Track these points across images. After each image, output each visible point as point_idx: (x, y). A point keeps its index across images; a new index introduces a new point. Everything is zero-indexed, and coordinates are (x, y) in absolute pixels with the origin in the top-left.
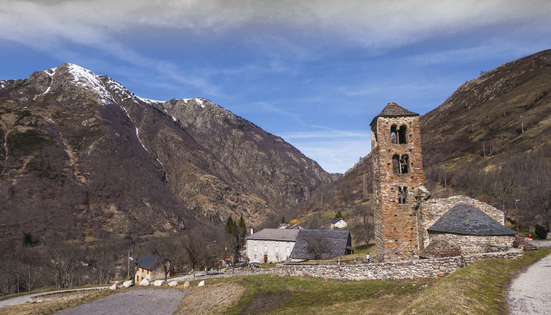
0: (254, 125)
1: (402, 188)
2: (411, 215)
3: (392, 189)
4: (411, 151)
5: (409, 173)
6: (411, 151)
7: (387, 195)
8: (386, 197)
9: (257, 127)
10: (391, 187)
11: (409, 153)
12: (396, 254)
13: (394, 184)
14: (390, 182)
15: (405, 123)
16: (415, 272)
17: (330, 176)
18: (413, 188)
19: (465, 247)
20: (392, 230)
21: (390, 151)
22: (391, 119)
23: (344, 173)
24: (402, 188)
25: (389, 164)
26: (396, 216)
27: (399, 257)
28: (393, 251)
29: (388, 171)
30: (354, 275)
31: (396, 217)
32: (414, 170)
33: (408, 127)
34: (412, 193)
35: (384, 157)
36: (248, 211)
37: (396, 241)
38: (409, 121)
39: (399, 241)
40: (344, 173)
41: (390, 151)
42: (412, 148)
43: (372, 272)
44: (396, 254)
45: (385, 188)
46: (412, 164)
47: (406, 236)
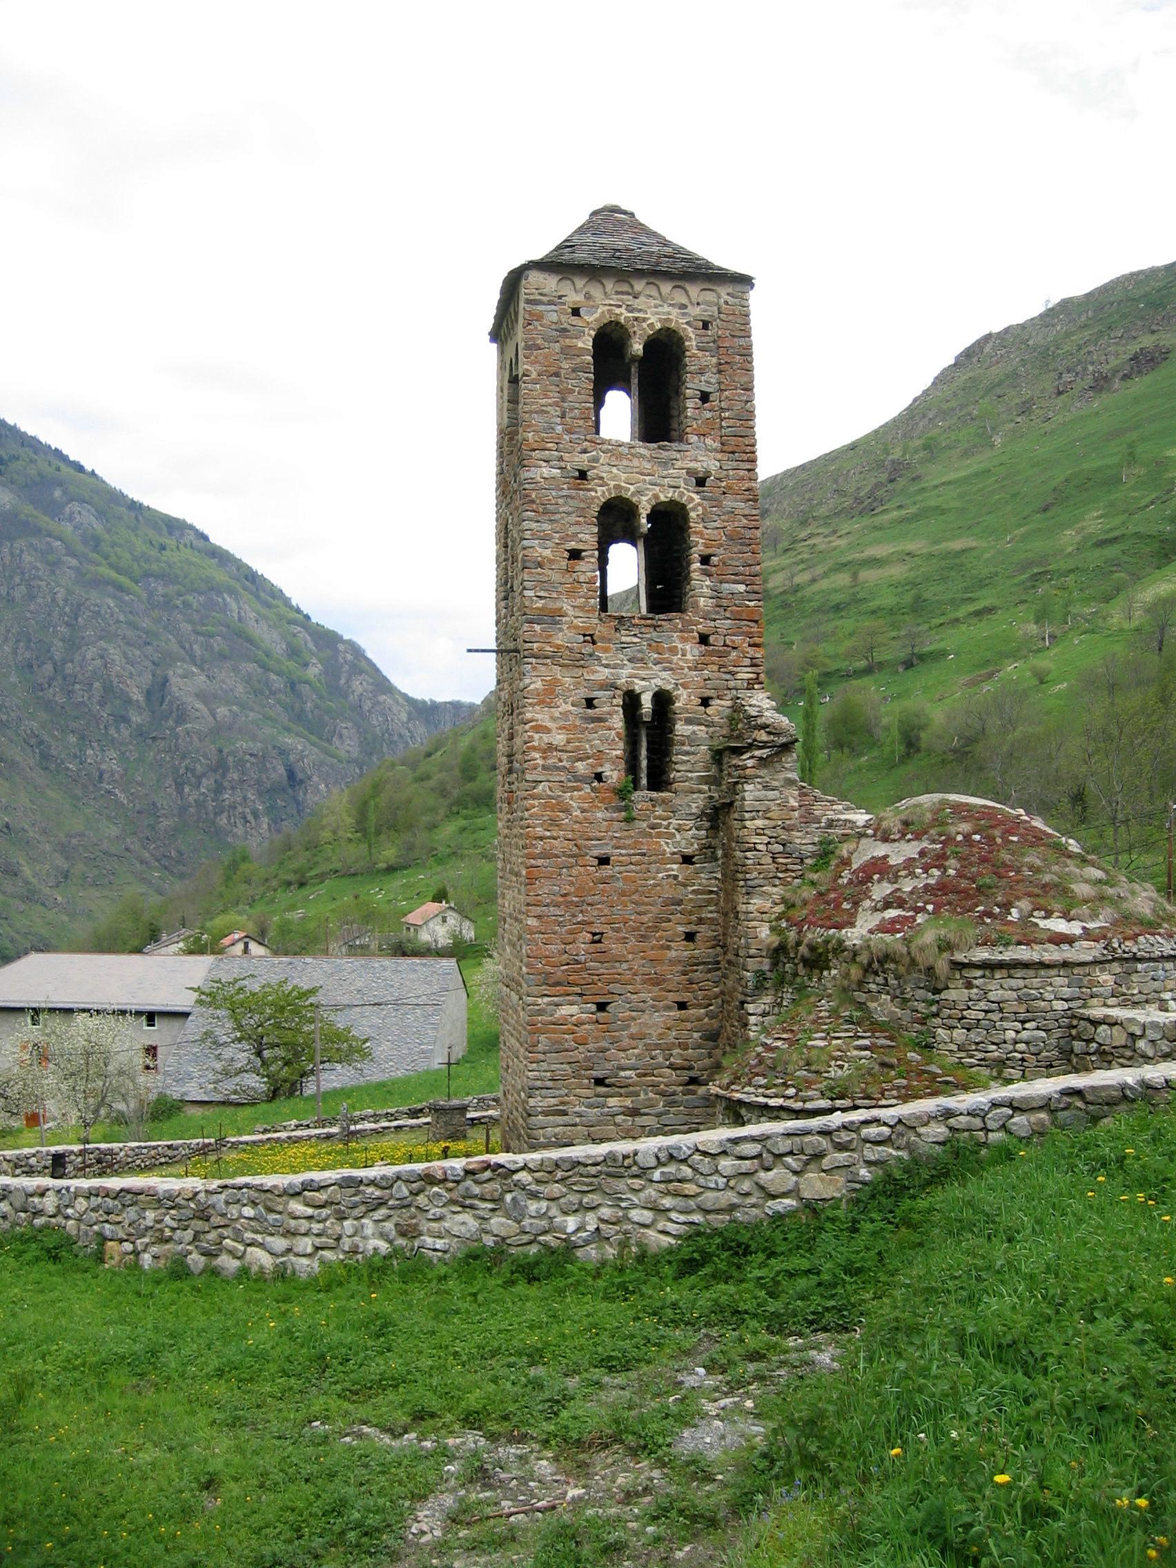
0: (65, 459)
1: (647, 701)
2: (687, 859)
3: (590, 703)
4: (701, 482)
5: (689, 615)
6: (701, 482)
7: (559, 739)
8: (551, 748)
9: (79, 468)
10: (583, 693)
11: (693, 499)
12: (600, 1082)
13: (603, 674)
14: (579, 662)
15: (677, 320)
16: (647, 1216)
17: (427, 712)
18: (705, 702)
19: (959, 1034)
20: (582, 946)
21: (583, 475)
22: (596, 291)
23: (478, 702)
24: (647, 701)
25: (575, 555)
26: (604, 861)
27: (612, 1102)
28: (579, 1068)
29: (571, 593)
30: (279, 1243)
31: (607, 871)
32: (717, 595)
33: (692, 344)
34: (701, 731)
35: (546, 512)
36: (27, 871)
37: (602, 1007)
38: (695, 311)
39: (618, 1009)
40: (478, 702)
41: (583, 475)
42: (713, 466)
43: (389, 1226)
44: (600, 1082)
45: (547, 697)
46: (705, 560)
47: (657, 981)
